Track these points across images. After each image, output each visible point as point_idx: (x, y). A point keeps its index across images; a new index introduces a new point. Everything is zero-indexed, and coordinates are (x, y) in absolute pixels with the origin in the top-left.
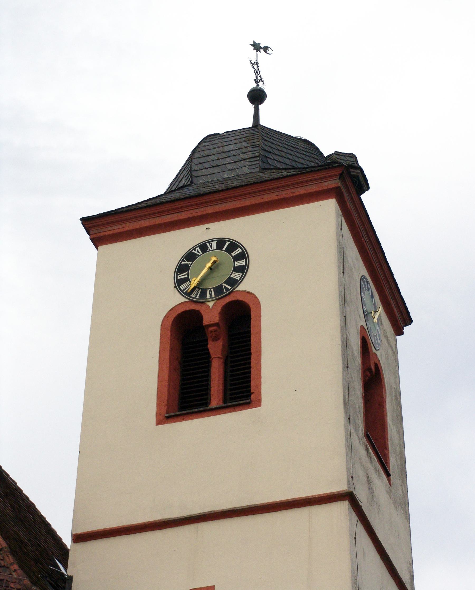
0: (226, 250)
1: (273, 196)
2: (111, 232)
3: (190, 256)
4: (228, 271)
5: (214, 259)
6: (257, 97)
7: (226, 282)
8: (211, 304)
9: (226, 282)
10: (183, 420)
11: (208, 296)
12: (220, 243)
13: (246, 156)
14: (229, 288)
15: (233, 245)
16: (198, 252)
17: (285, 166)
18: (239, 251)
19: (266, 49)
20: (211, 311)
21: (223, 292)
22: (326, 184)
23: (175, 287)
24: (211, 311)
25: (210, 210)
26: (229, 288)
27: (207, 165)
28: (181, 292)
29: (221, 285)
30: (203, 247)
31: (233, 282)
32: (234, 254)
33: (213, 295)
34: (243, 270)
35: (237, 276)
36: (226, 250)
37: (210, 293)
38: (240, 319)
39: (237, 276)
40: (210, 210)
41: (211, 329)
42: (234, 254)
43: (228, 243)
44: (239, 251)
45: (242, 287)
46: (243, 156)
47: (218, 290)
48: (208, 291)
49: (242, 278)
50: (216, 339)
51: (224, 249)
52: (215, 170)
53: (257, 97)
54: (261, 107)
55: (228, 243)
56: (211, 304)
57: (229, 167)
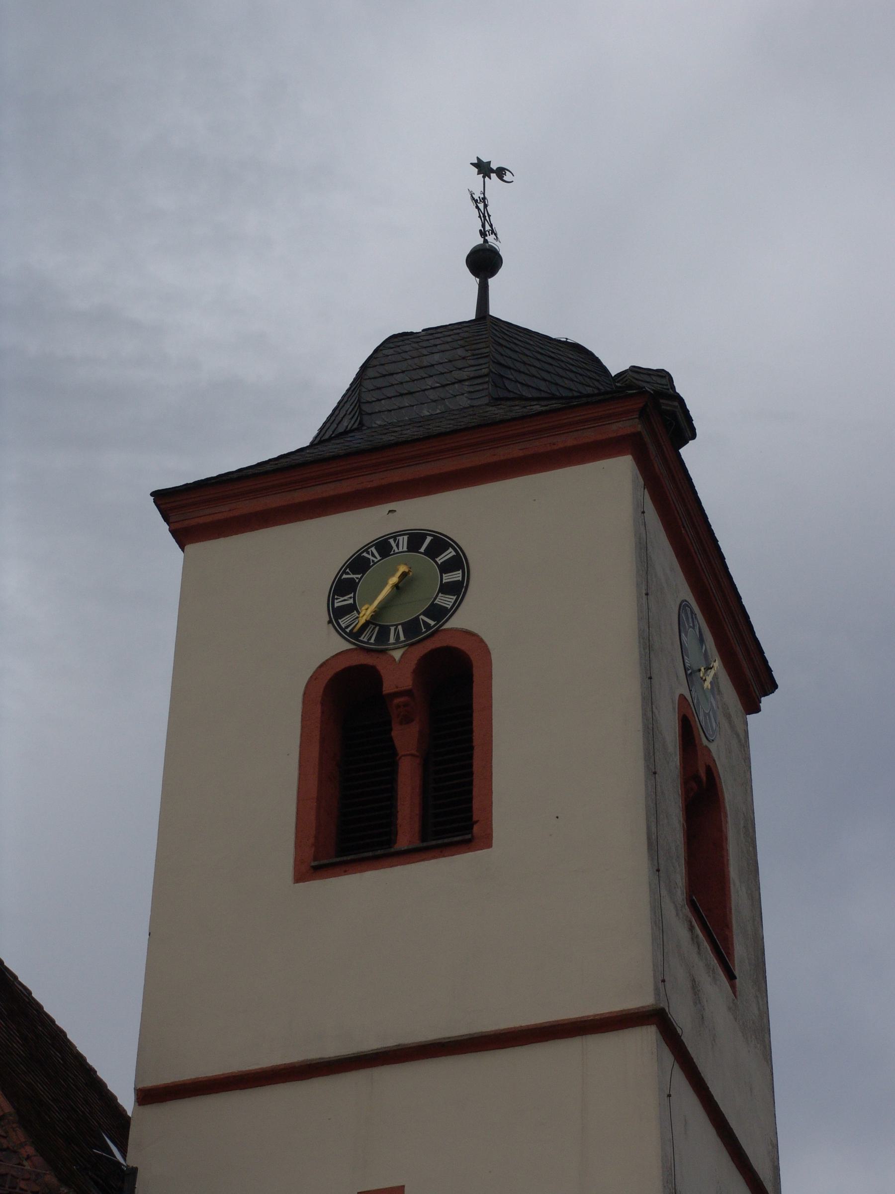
0: (426, 553)
1: (514, 451)
2: (209, 519)
3: (358, 564)
4: (429, 591)
5: (402, 569)
6: (484, 262)
7: (425, 613)
8: (397, 654)
9: (425, 613)
10: (346, 872)
11: (392, 640)
12: (415, 539)
13: (464, 375)
14: (432, 623)
15: (440, 543)
16: (374, 555)
17: (536, 394)
18: (450, 553)
19: (501, 172)
20: (398, 667)
21: (419, 632)
22: (614, 427)
23: (330, 622)
24: (398, 667)
25: (396, 476)
26: (432, 623)
27: (390, 392)
28: (341, 631)
29: (417, 618)
30: (383, 546)
31: (438, 613)
32: (440, 560)
33: (402, 638)
34: (458, 589)
35: (447, 601)
36: (426, 553)
37: (396, 634)
38: (453, 682)
39: (447, 601)
40: (396, 476)
41: (397, 701)
42: (440, 560)
43: (429, 539)
44: (450, 553)
45: (454, 623)
46: (458, 375)
47: (412, 627)
48: (393, 629)
49: (457, 606)
50: (407, 720)
51: (422, 550)
52: (406, 401)
53: (484, 262)
54: (493, 282)
55: (429, 539)
56: (397, 654)
57: (432, 395)
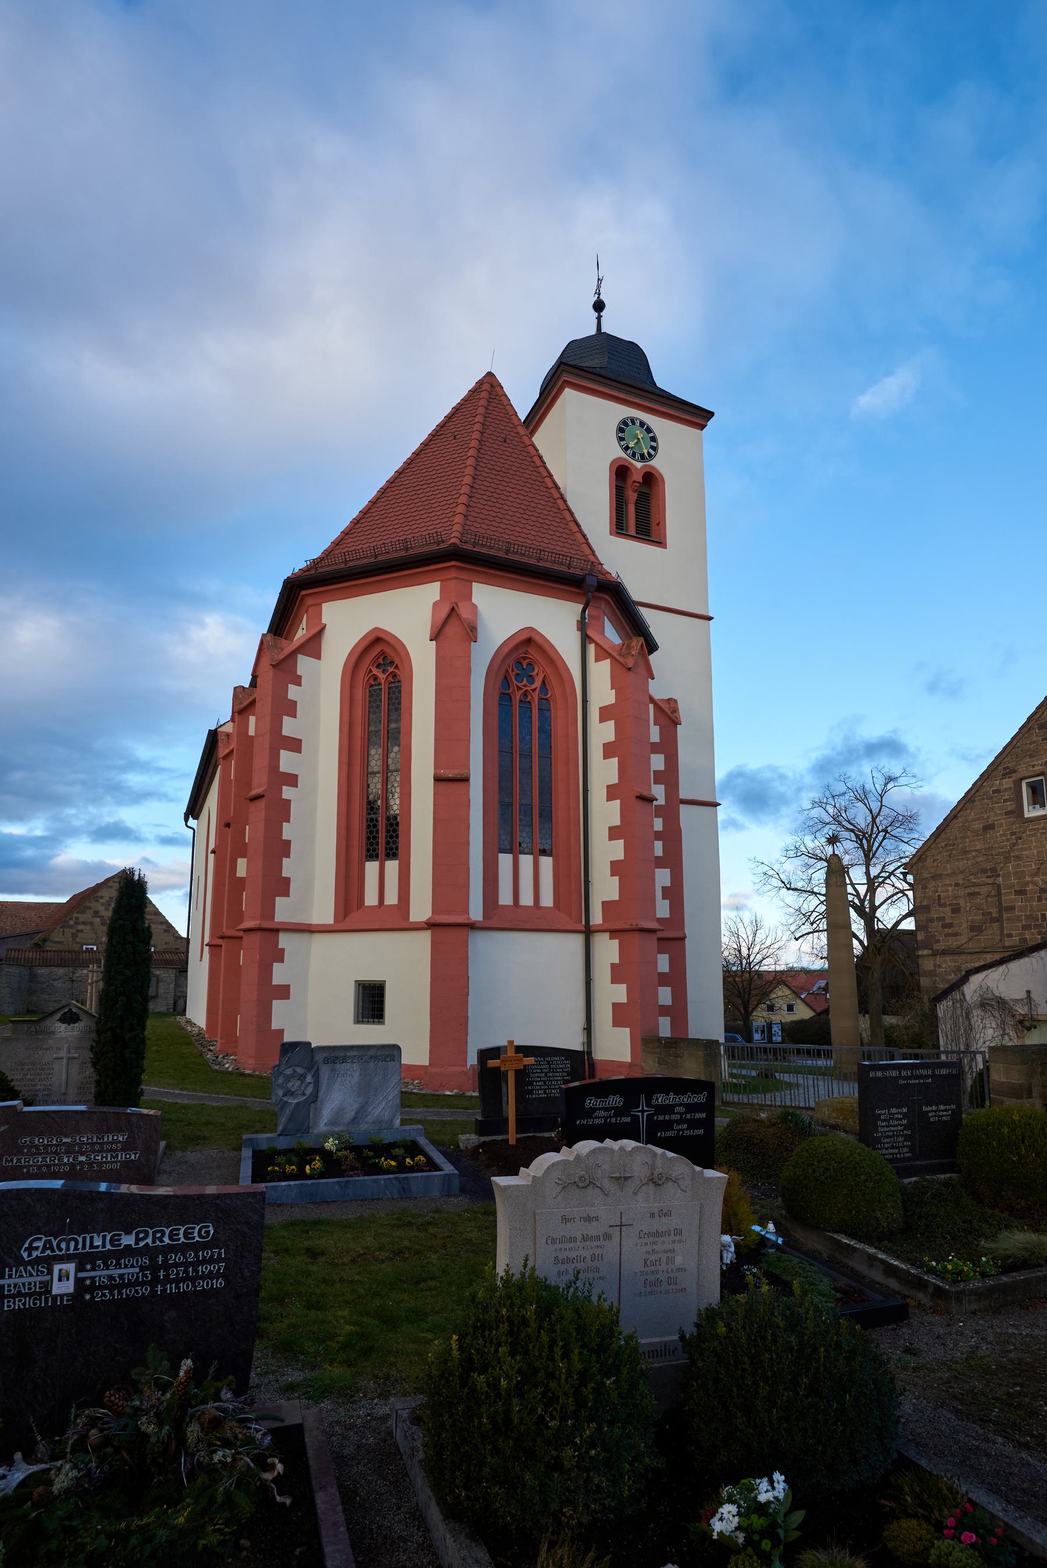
3: (624, 422)
12: (642, 424)
15: (649, 430)
28: (621, 446)
30: (633, 421)
